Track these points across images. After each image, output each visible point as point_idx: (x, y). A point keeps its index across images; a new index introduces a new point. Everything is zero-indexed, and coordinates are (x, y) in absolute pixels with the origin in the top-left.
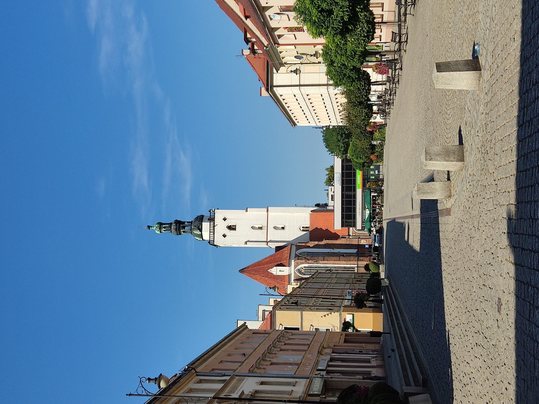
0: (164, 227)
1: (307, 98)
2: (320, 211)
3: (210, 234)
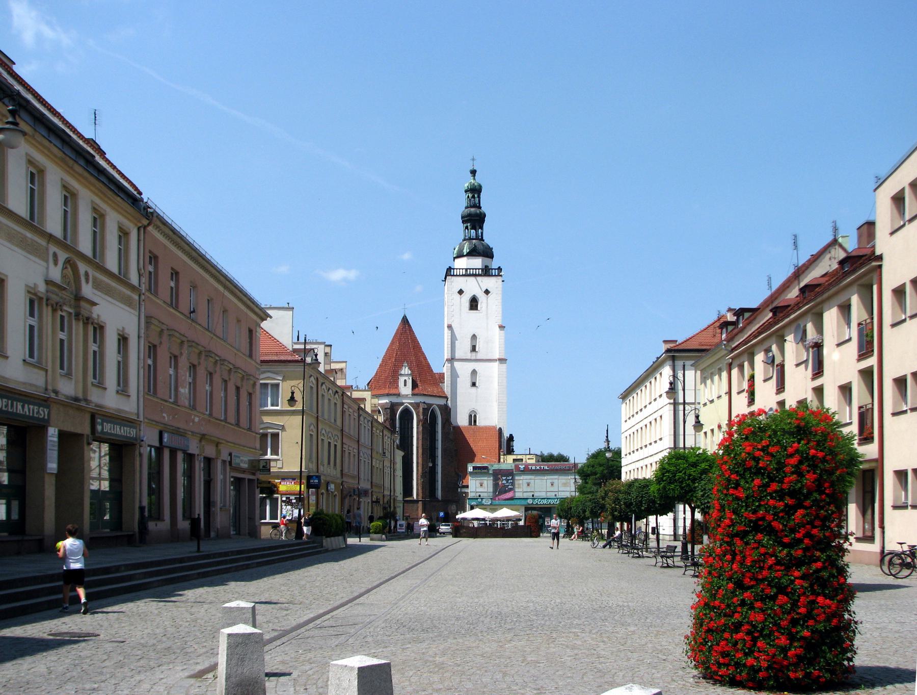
0: (473, 197)
1: (657, 415)
2: (500, 442)
3: (463, 269)
